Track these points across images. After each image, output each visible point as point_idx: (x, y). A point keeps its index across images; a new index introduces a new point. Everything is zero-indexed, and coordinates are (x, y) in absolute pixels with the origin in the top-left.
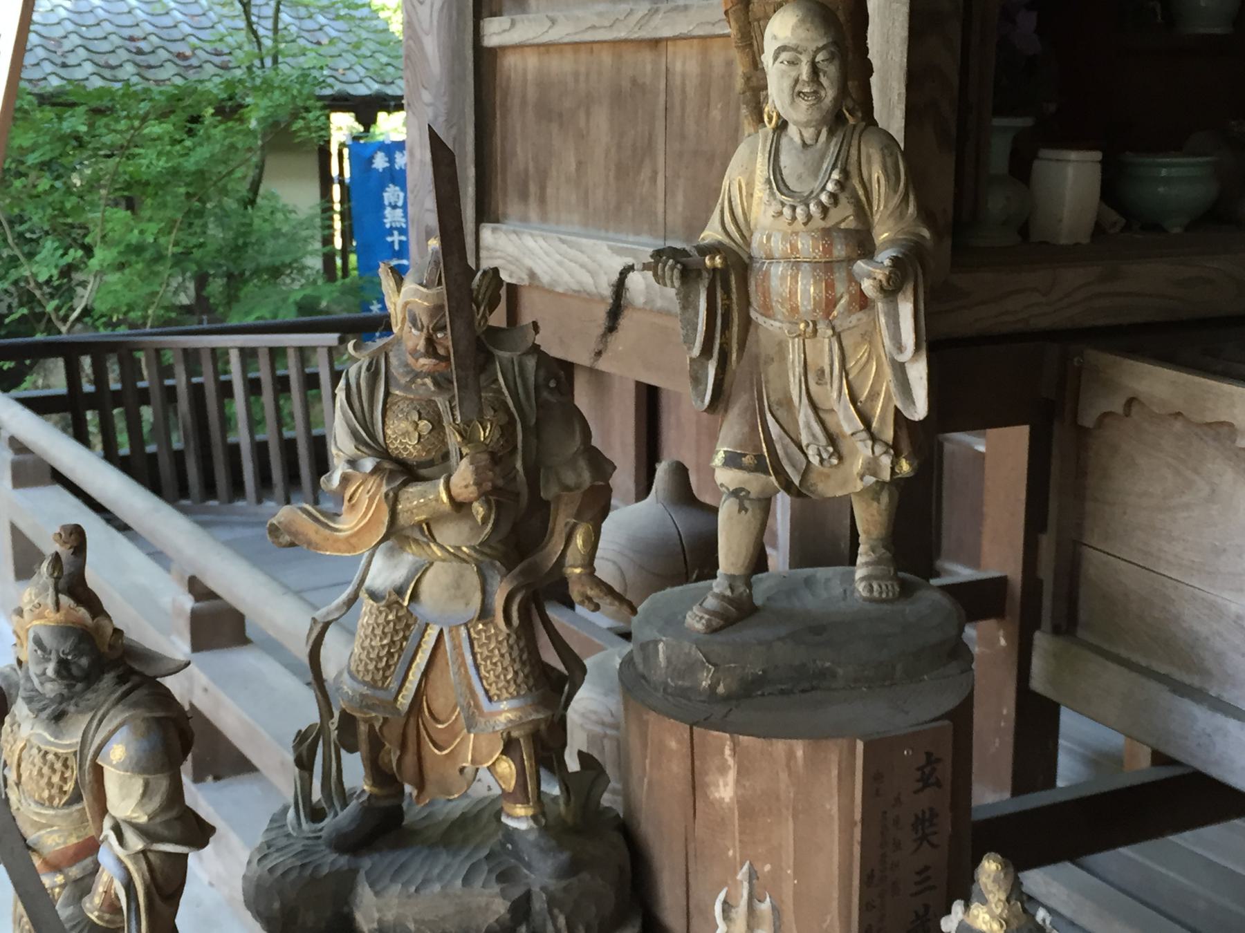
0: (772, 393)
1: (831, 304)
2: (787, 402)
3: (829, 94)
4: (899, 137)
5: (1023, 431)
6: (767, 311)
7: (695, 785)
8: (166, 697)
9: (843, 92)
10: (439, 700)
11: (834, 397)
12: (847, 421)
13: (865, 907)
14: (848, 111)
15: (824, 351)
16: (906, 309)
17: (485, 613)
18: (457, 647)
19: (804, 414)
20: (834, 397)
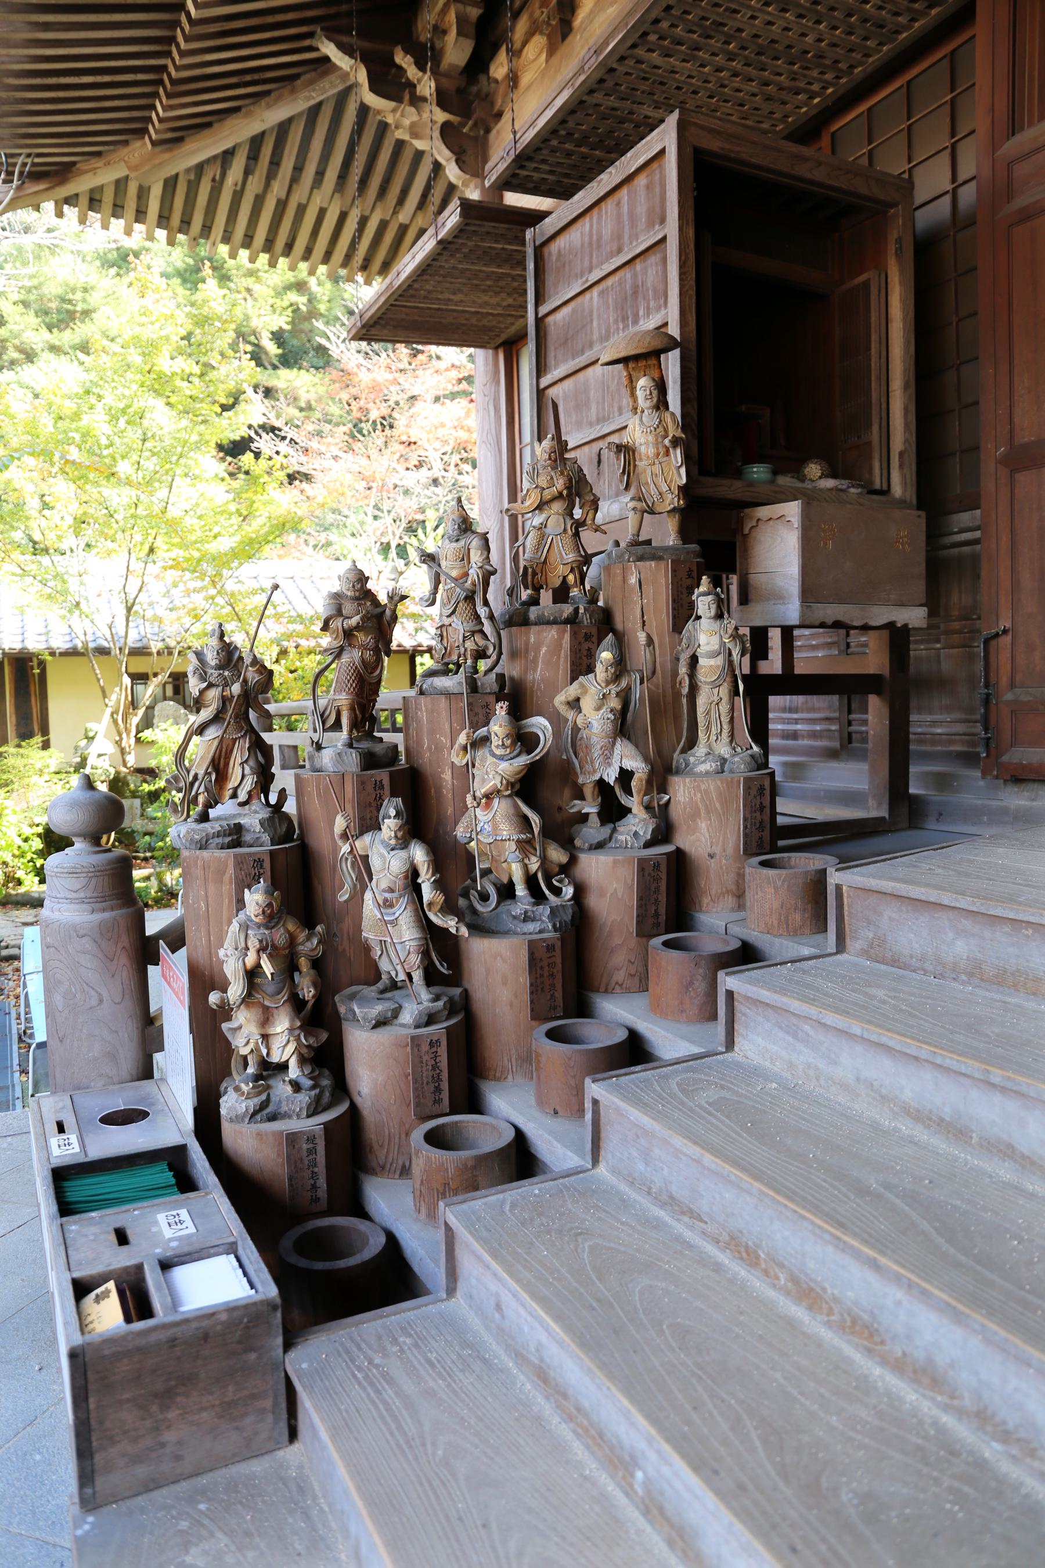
0: (643, 481)
1: (658, 454)
2: (647, 483)
3: (655, 400)
4: (504, 47)
5: (797, 671)
6: (641, 460)
7: (624, 580)
8: (379, 661)
9: (659, 400)
10: (551, 559)
11: (660, 480)
12: (664, 488)
13: (674, 609)
14: (661, 404)
15: (657, 469)
16: (678, 451)
17: (565, 530)
18: (558, 542)
19: (652, 486)
20: (660, 480)
